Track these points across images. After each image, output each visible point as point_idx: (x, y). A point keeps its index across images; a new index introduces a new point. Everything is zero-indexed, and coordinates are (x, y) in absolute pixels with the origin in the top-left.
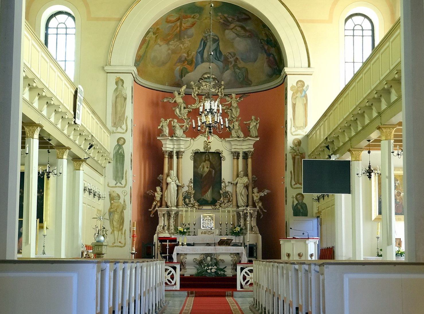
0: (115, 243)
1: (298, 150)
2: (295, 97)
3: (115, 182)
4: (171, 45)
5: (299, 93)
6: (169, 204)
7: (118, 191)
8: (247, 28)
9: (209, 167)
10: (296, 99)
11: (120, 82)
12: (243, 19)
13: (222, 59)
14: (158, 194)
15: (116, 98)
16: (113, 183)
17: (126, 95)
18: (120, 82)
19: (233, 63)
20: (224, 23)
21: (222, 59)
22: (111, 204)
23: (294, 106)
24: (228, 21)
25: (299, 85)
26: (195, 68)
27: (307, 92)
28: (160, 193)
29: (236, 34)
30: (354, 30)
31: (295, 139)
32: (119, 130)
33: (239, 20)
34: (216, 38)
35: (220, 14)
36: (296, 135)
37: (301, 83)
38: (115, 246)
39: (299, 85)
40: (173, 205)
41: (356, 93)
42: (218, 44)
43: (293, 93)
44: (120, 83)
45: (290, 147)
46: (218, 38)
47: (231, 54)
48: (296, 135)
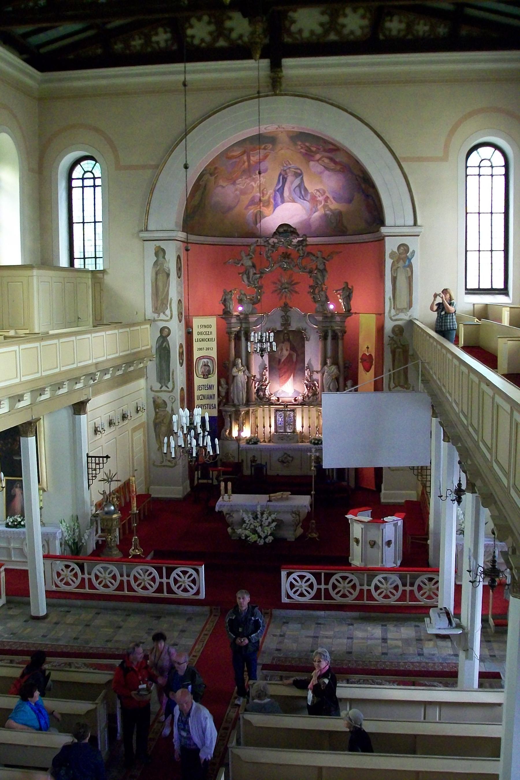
0: (163, 462)
1: (400, 341)
2: (395, 268)
3: (160, 385)
4: (239, 184)
5: (401, 261)
6: (236, 401)
7: (164, 396)
8: (337, 160)
9: (289, 349)
10: (397, 270)
11: (160, 252)
12: (330, 149)
13: (309, 197)
14: (222, 387)
15: (157, 274)
16: (157, 386)
17: (169, 270)
18: (160, 252)
19: (323, 203)
20: (306, 154)
21: (309, 197)
22: (156, 413)
23: (394, 280)
24: (312, 151)
25: (401, 251)
26: (274, 210)
27: (413, 261)
28: (225, 386)
29: (324, 167)
30: (479, 167)
31: (395, 326)
32: (162, 316)
33: (325, 151)
34: (299, 171)
35: (299, 143)
36: (396, 320)
37: (404, 248)
38: (164, 466)
39: (401, 251)
40: (241, 403)
41: (453, 370)
42: (302, 179)
43: (393, 262)
44: (161, 255)
45: (389, 336)
46: (301, 171)
47: (319, 192)
48: (396, 320)
